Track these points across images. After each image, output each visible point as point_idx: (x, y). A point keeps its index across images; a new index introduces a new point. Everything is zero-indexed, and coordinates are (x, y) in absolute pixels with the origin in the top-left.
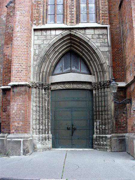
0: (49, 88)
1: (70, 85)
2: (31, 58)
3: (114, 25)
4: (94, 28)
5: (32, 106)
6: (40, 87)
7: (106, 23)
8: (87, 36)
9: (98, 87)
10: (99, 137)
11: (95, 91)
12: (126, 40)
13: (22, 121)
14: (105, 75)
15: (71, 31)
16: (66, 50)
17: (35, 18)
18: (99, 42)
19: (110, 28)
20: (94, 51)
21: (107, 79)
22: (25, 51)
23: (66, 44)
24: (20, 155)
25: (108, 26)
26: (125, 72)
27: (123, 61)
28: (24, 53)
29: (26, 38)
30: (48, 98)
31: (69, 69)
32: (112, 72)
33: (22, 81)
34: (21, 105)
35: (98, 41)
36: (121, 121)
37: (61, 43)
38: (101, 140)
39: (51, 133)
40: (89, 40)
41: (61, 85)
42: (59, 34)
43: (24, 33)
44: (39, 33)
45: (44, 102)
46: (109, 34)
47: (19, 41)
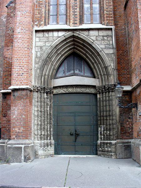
0: (52, 92)
1: (73, 89)
2: (32, 60)
3: (119, 26)
4: (98, 29)
5: (33, 111)
6: (41, 91)
7: (110, 24)
8: (91, 37)
9: (102, 91)
10: (104, 143)
11: (100, 96)
12: (131, 42)
13: (23, 127)
14: (110, 78)
15: (74, 32)
16: (69, 52)
17: (37, 19)
18: (103, 44)
19: (115, 29)
20: (98, 53)
21: (112, 82)
22: (26, 53)
23: (69, 46)
24: (21, 162)
25: (113, 27)
26: (131, 76)
27: (129, 64)
28: (26, 56)
29: (27, 39)
30: (51, 102)
31: (72, 72)
32: (117, 76)
33: (23, 85)
34: (22, 109)
35: (102, 43)
36: (127, 126)
37: (63, 45)
38: (106, 146)
39: (54, 139)
40: (92, 41)
41: (64, 89)
42: (62, 36)
43: (26, 34)
44: (41, 35)
45: (46, 106)
46: (114, 36)
47: (20, 43)
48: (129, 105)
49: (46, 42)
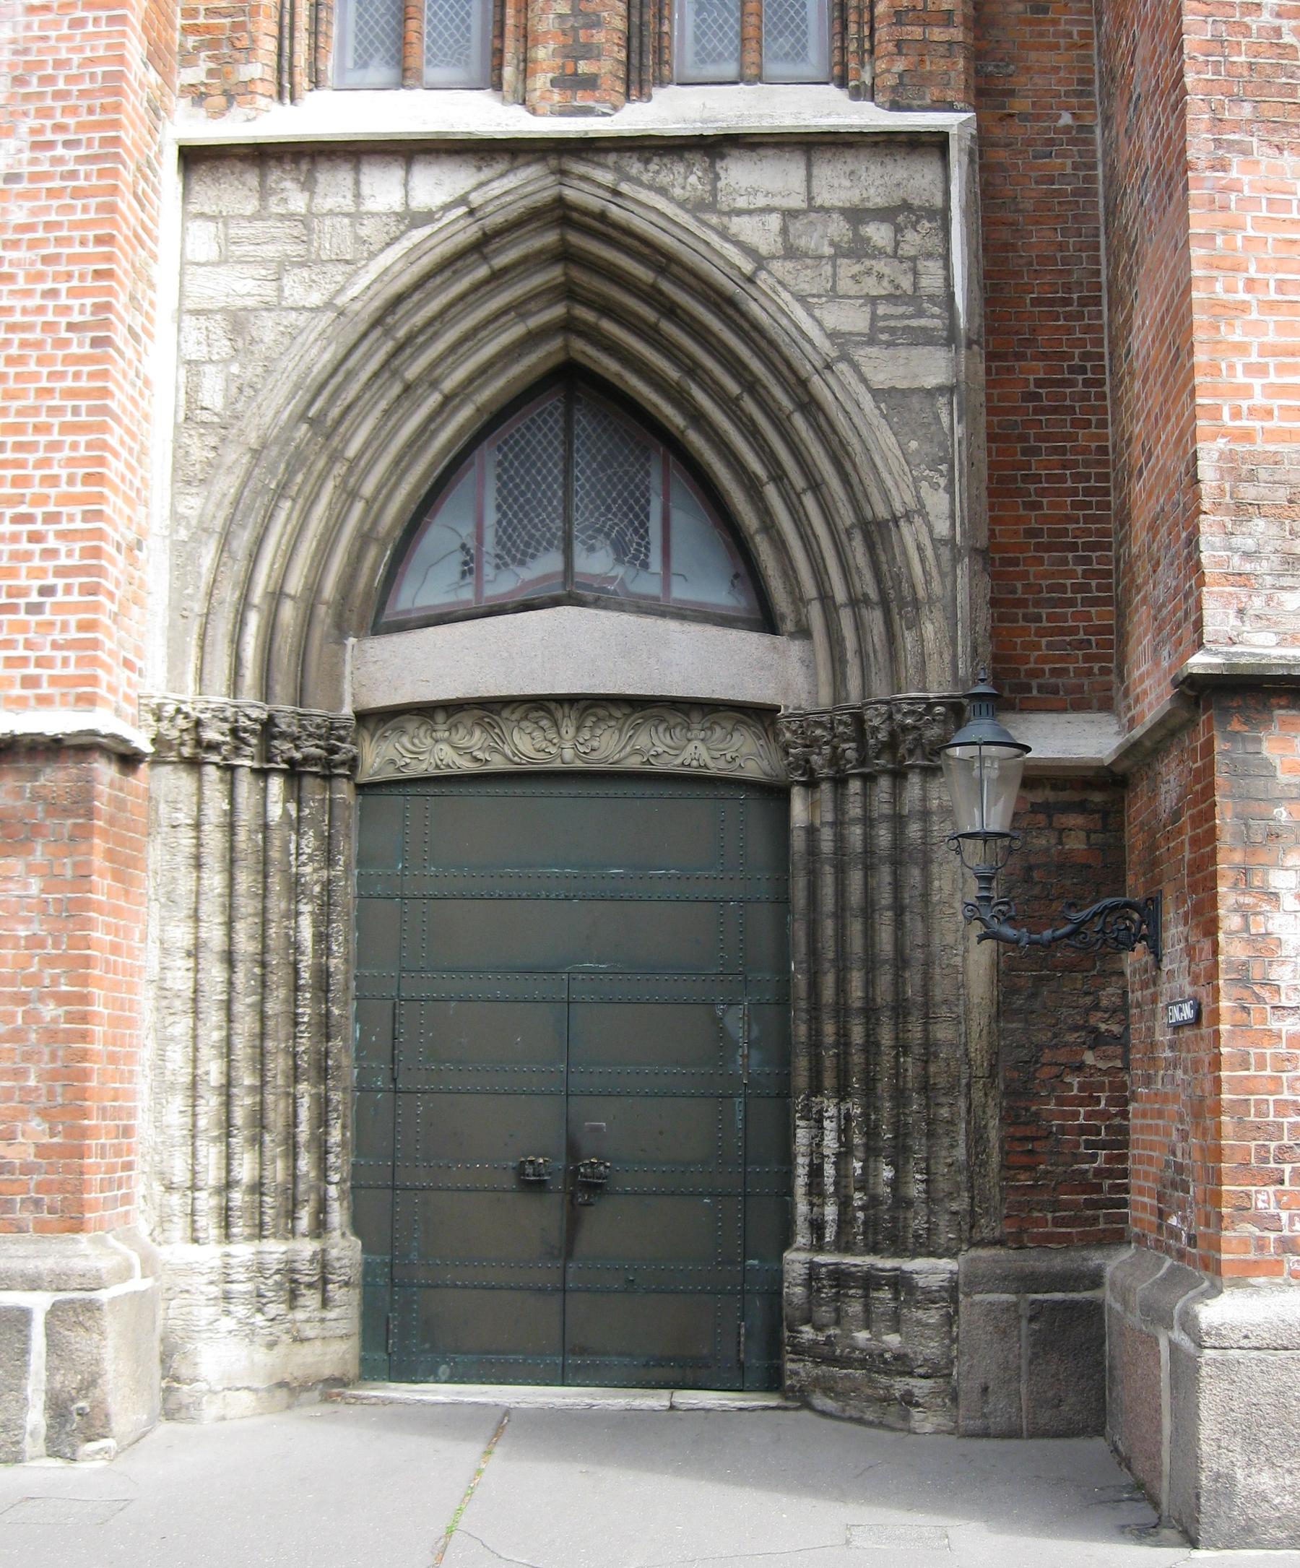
0: (343, 763)
1: (552, 735)
2: (144, 451)
3: (1020, 105)
4: (812, 145)
5: (154, 950)
6: (237, 751)
7: (932, 93)
8: (738, 225)
9: (835, 759)
10: (840, 1277)
11: (813, 806)
12: (1131, 280)
13: (44, 1114)
14: (909, 638)
15: (563, 172)
16: (516, 370)
17: (194, 29)
18: (852, 288)
19: (983, 143)
20: (804, 383)
21: (932, 676)
22: (83, 383)
23: (518, 309)
24: (16, 1458)
25: (955, 122)
26: (1122, 616)
27: (1106, 492)
28: (76, 411)
29: (91, 249)
30: (330, 862)
31: (550, 563)
32: (984, 614)
33: (44, 701)
34: (35, 942)
35: (845, 285)
36: (1064, 1115)
37: (462, 297)
38: (855, 1308)
39: (357, 1225)
40: (748, 267)
41: (460, 737)
42: (446, 208)
43: (77, 193)
44: (232, 194)
45: (278, 905)
46: (966, 212)
47: (21, 284)
48: (1076, 916)
49: (282, 267)
